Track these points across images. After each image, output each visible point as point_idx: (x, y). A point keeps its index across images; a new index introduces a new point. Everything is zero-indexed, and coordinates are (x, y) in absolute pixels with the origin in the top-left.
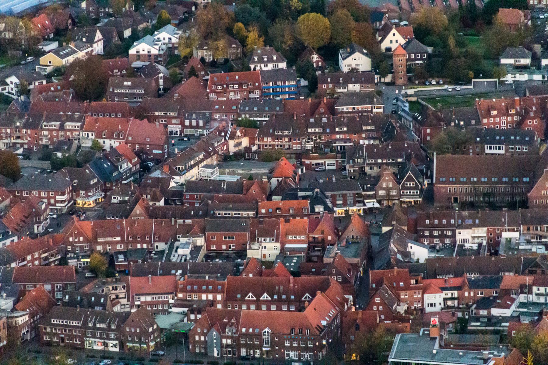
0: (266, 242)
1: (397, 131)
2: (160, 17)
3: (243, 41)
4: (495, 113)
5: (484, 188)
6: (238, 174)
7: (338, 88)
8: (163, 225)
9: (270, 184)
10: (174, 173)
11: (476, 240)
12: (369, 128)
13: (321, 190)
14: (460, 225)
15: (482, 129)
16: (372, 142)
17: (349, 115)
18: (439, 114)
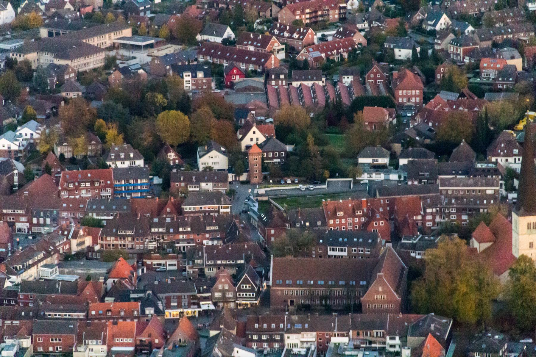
0: (93, 345)
1: (239, 232)
2: (26, 112)
3: (103, 137)
4: (341, 214)
5: (321, 291)
6: (77, 274)
7: (190, 187)
8: (309, 320)
9: (106, 284)
10: (10, 272)
11: (305, 345)
12: (212, 228)
13: (153, 292)
14: (289, 329)
15: (325, 231)
16: (215, 242)
17: (192, 215)
18: (285, 215)
